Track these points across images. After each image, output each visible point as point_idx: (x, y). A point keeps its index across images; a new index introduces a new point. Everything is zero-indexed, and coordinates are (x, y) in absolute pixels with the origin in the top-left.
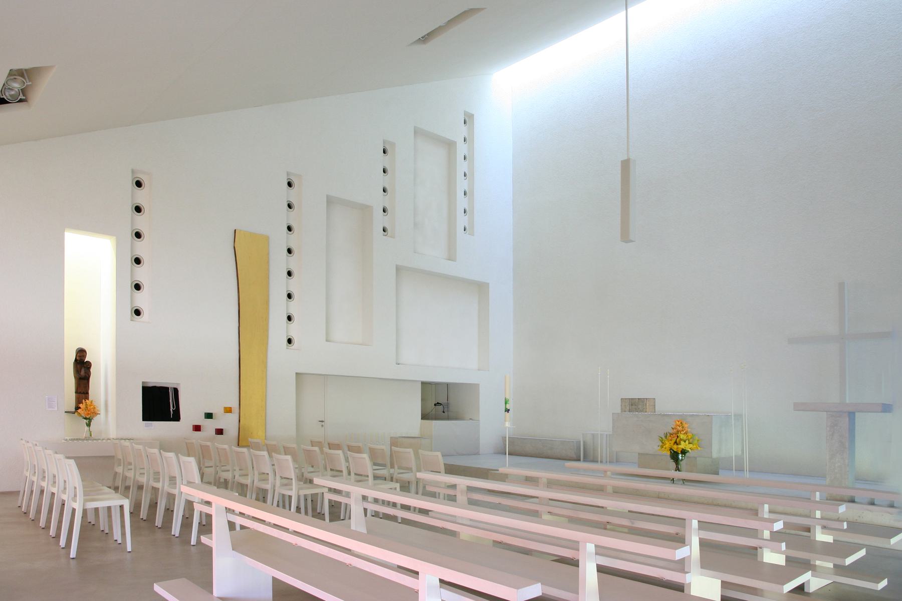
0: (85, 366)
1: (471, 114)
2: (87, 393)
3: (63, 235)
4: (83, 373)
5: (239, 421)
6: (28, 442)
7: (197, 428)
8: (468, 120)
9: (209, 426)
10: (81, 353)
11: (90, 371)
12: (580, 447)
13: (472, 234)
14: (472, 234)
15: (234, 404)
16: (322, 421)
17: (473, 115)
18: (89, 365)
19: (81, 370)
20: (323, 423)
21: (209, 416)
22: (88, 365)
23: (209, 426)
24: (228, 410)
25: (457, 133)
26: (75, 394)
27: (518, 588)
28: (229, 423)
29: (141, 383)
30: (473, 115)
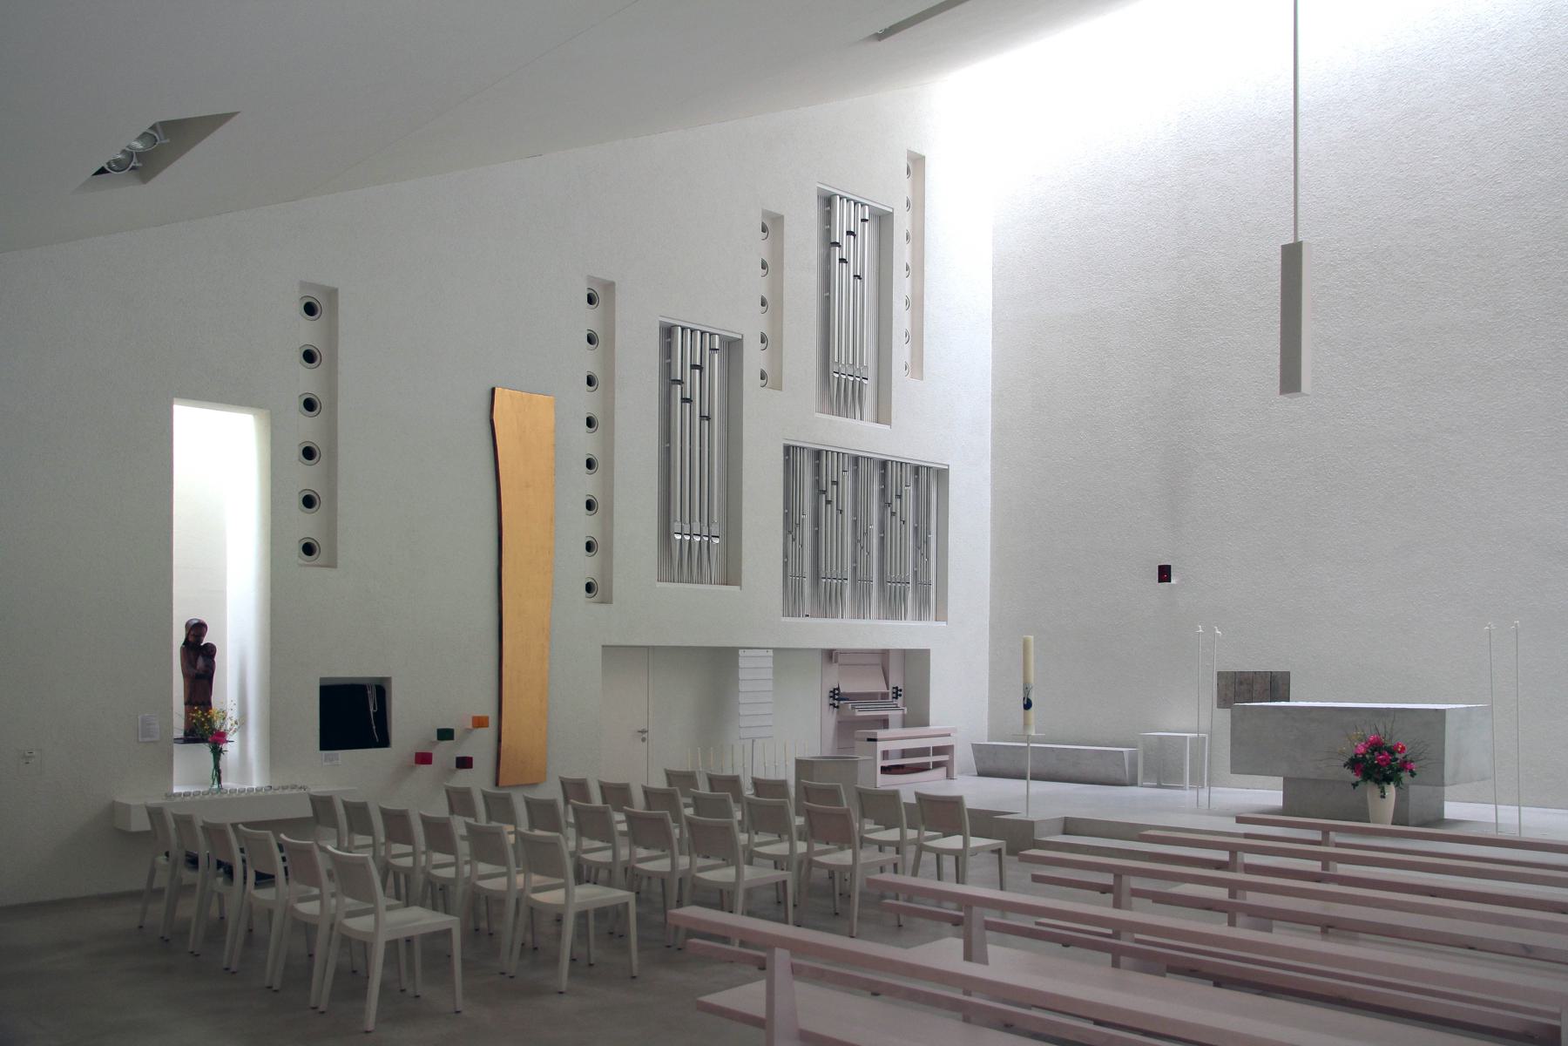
0: (204, 652)
1: (920, 155)
2: (209, 703)
3: (986, 948)
4: (201, 662)
5: (499, 740)
6: (1384, 361)
7: (424, 758)
8: (916, 165)
9: (444, 753)
10: (197, 630)
11: (214, 661)
12: (1382, 823)
13: (607, 600)
14: (607, 600)
15: (489, 711)
16: (643, 732)
17: (924, 157)
18: (212, 651)
19: (196, 659)
20: (645, 735)
21: (445, 734)
22: (210, 651)
23: (444, 753)
24: (480, 722)
25: (894, 199)
26: (183, 706)
27: (907, 948)
28: (479, 746)
29: (318, 681)
30: (923, 158)
